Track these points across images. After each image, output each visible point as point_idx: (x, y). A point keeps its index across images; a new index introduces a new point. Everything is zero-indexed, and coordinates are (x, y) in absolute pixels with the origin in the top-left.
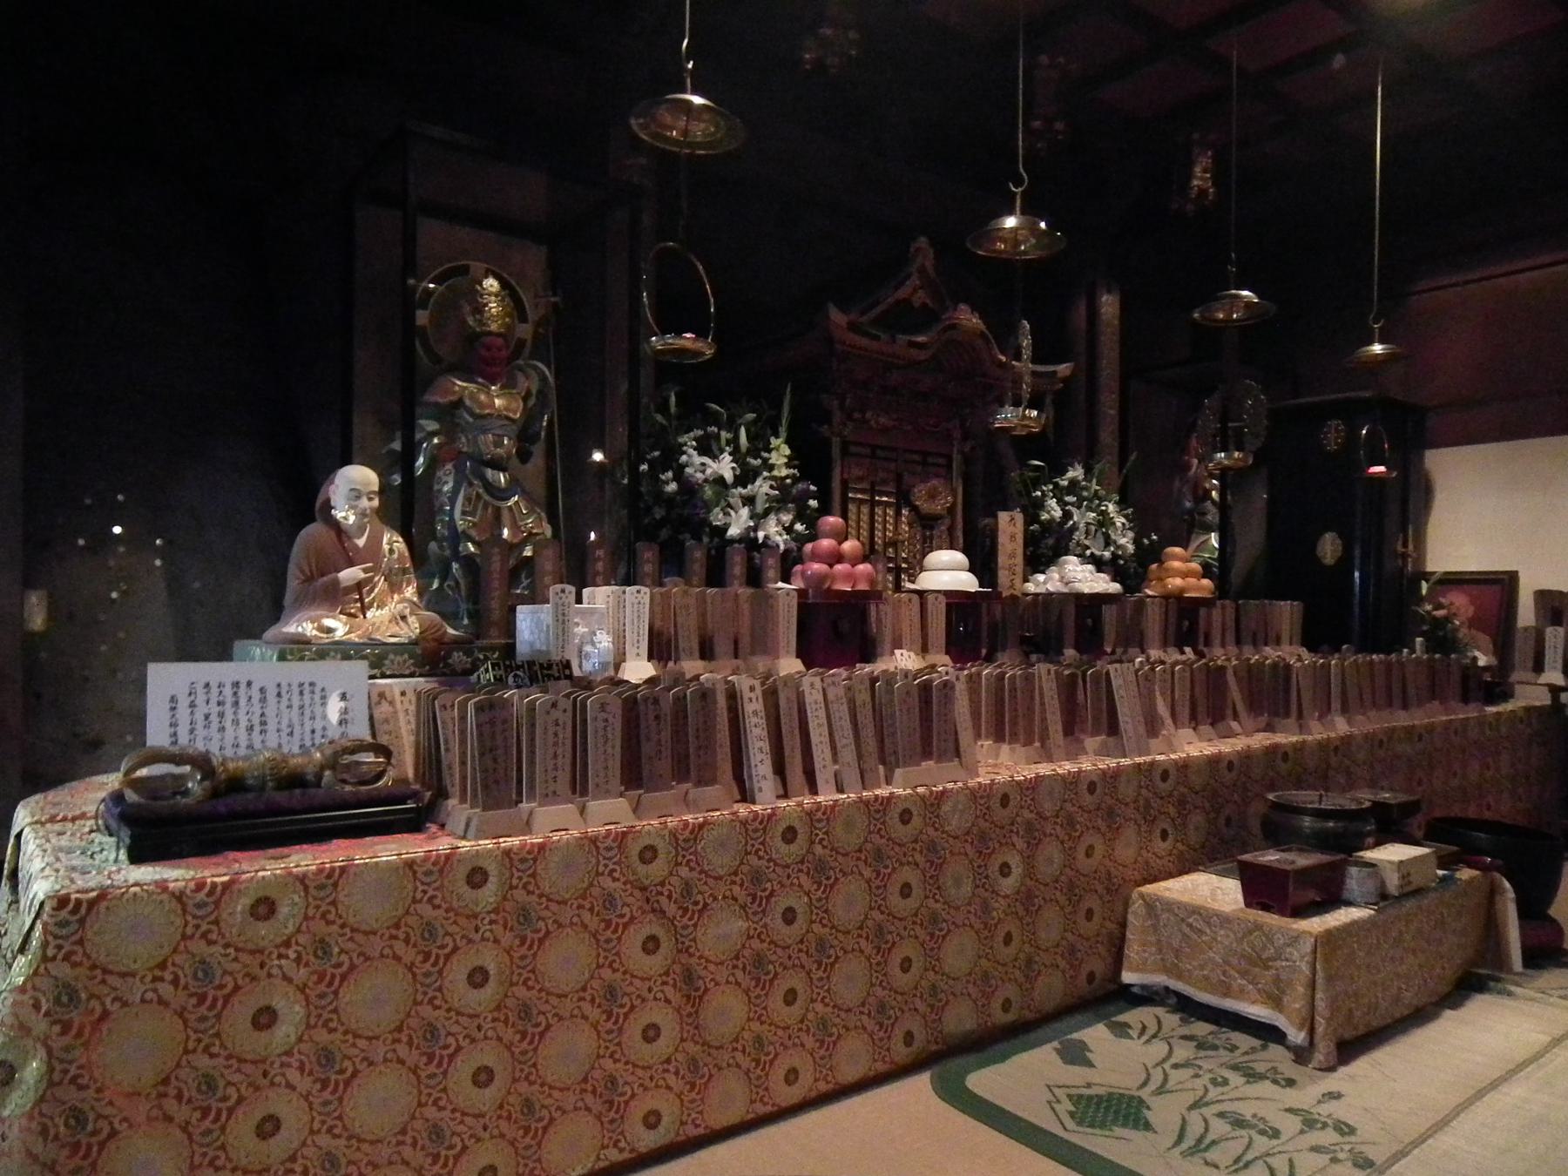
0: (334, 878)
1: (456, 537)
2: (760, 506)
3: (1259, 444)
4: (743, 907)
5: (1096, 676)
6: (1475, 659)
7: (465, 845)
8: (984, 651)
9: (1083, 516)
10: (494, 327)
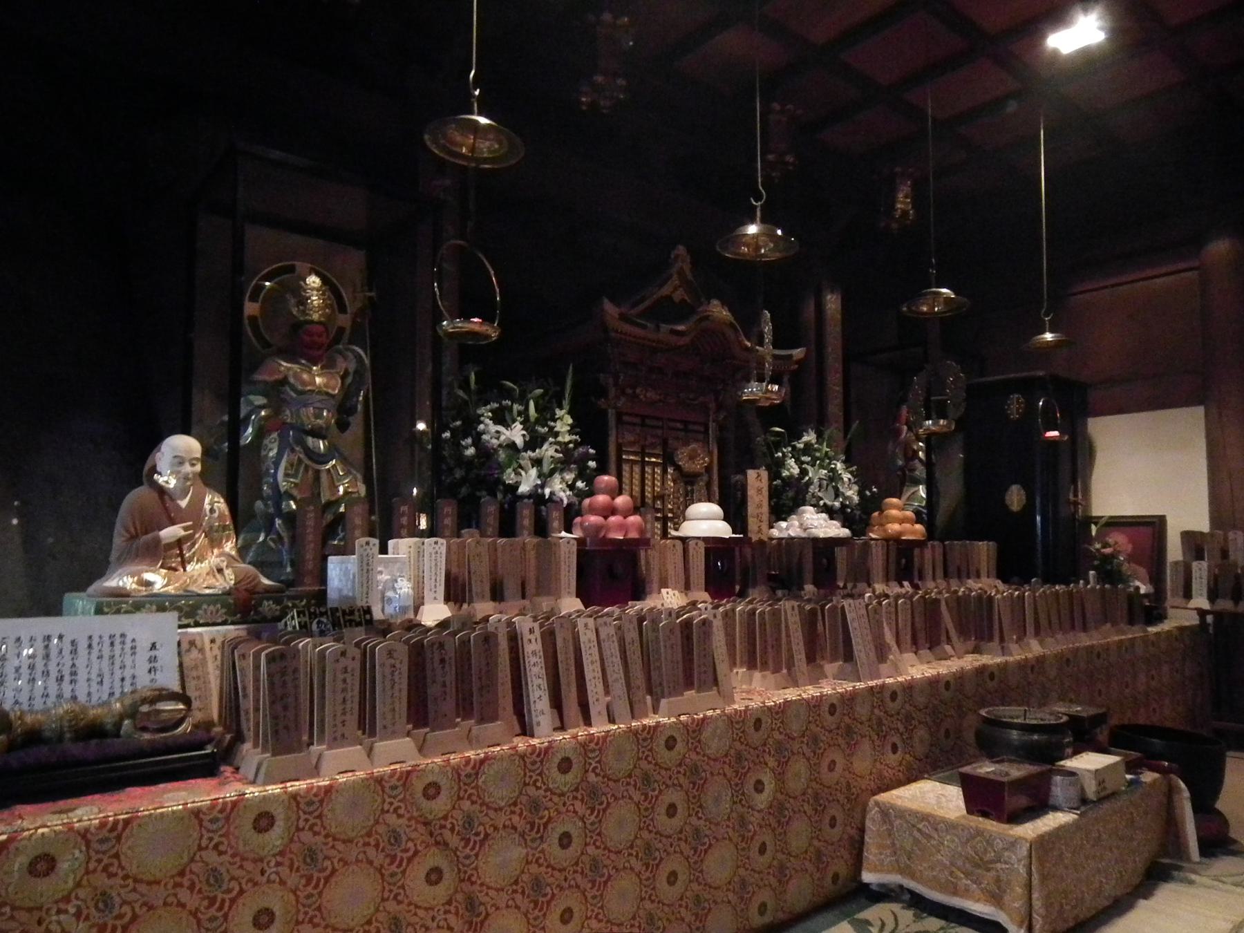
0: (116, 831)
1: (279, 496)
2: (546, 468)
3: (959, 414)
4: (522, 835)
5: (834, 608)
6: (1138, 588)
7: (252, 791)
8: (738, 588)
9: (816, 472)
10: (316, 317)
